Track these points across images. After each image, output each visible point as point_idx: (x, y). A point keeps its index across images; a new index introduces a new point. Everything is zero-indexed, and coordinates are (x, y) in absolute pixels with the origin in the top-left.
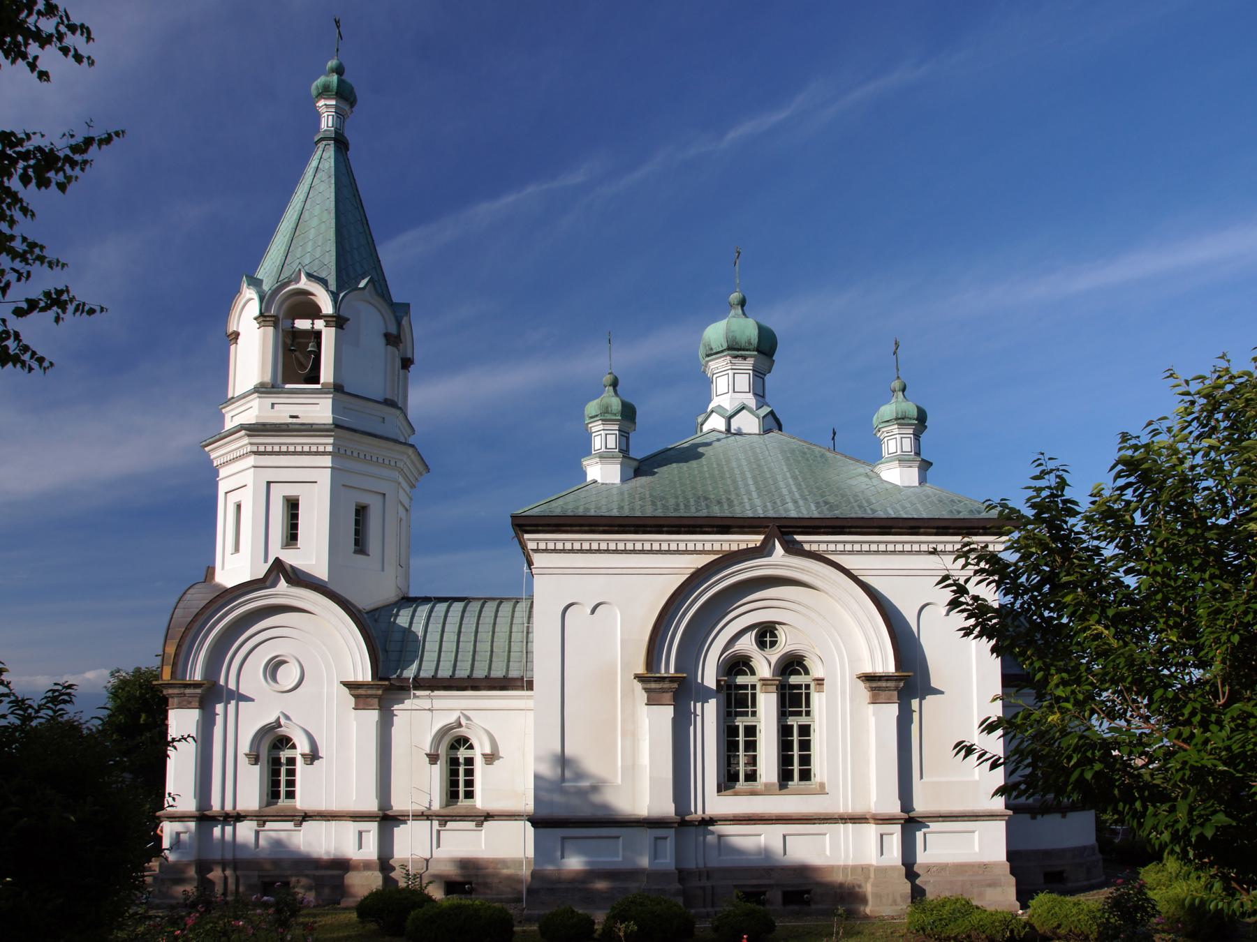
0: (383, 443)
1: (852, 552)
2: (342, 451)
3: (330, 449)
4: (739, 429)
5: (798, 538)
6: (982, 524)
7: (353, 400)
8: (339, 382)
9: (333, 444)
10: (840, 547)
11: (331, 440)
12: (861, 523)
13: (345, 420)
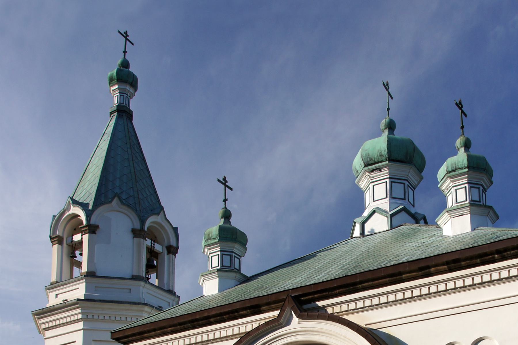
0: (115, 306)
1: (364, 309)
2: (90, 317)
3: (80, 316)
4: (372, 230)
5: (320, 303)
6: (494, 248)
7: (101, 280)
8: (93, 270)
9: (81, 313)
10: (352, 306)
11: (79, 310)
12: (370, 277)
13: (95, 295)
